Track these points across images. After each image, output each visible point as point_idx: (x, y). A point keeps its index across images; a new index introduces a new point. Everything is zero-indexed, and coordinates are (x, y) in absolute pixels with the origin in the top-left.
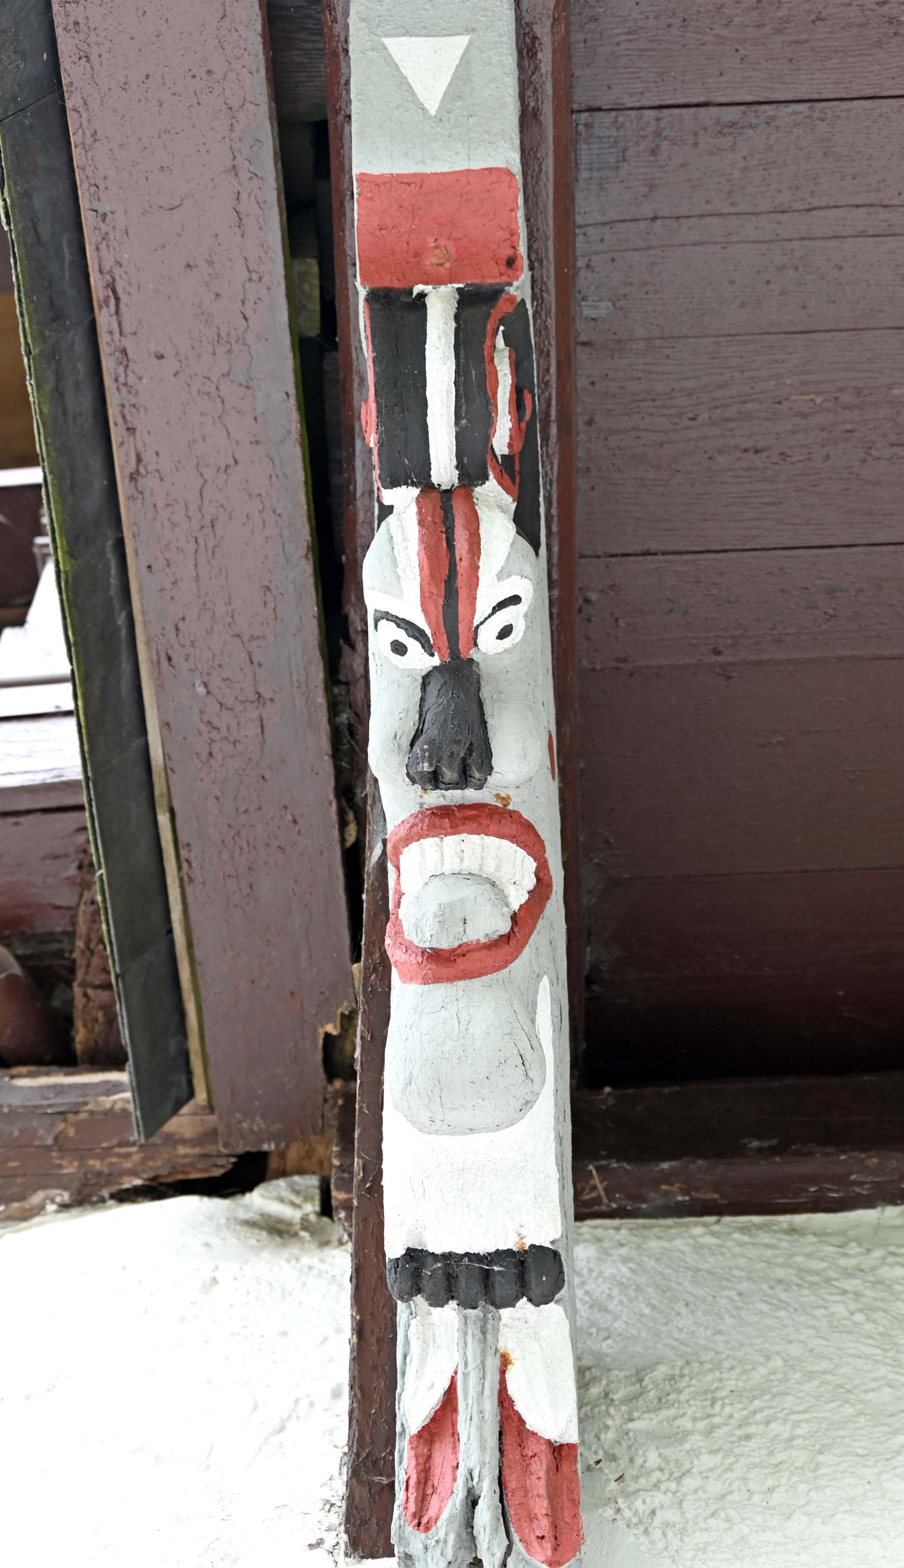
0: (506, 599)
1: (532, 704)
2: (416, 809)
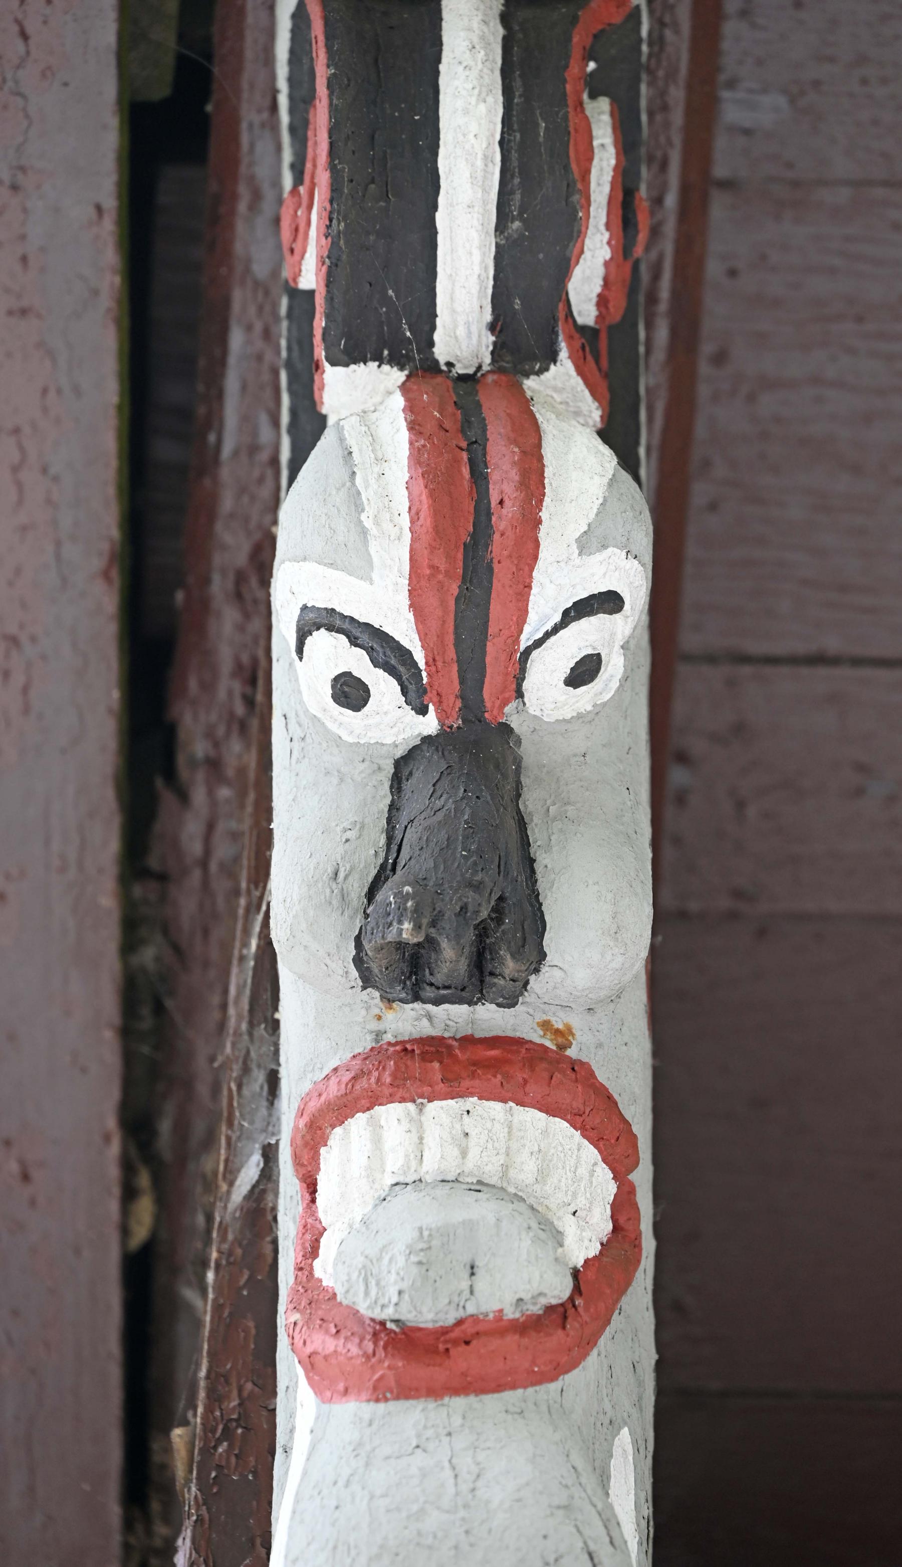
0: (592, 597)
1: (631, 832)
2: (366, 1044)
